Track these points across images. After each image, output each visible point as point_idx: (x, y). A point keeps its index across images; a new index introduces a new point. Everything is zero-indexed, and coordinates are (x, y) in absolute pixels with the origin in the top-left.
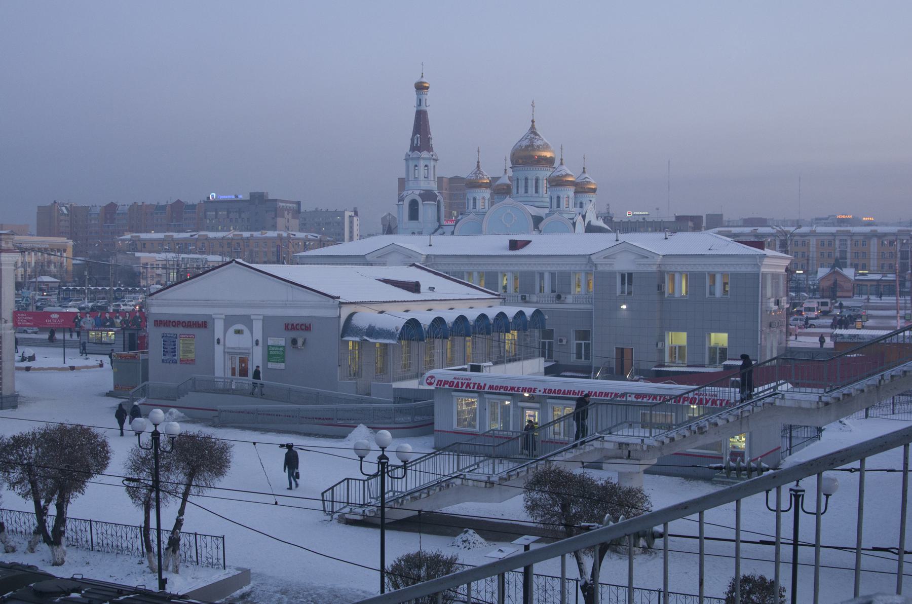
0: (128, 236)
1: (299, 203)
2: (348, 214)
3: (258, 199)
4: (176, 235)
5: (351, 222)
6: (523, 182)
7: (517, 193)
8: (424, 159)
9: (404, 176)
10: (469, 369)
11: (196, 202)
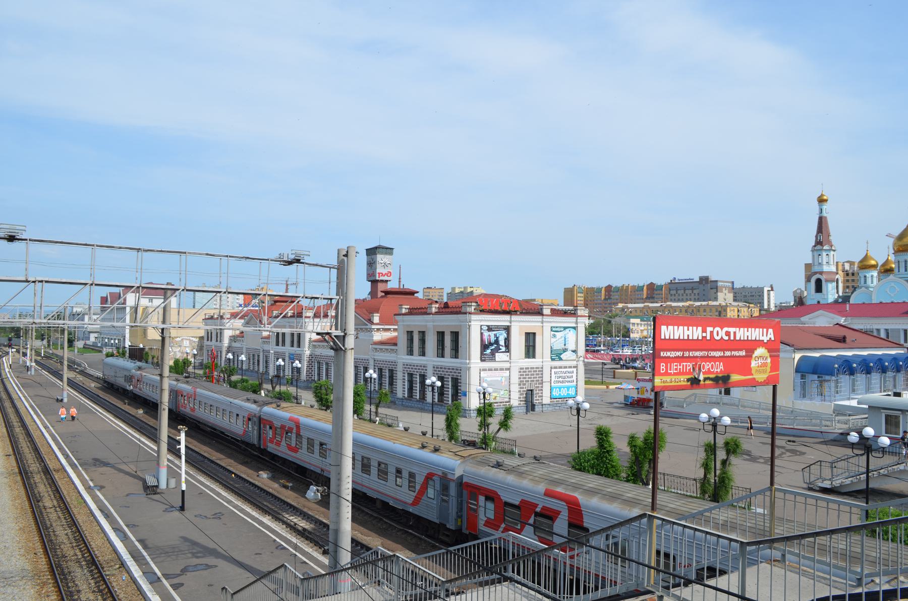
0: (620, 305)
1: (733, 283)
2: (766, 290)
3: (704, 280)
4: (651, 305)
5: (769, 295)
6: (903, 263)
7: (899, 271)
8: (825, 250)
9: (810, 261)
10: (893, 394)
11: (663, 283)
